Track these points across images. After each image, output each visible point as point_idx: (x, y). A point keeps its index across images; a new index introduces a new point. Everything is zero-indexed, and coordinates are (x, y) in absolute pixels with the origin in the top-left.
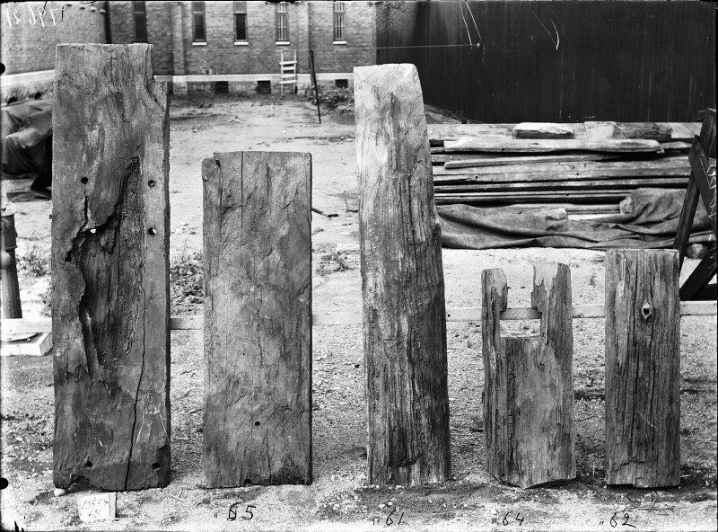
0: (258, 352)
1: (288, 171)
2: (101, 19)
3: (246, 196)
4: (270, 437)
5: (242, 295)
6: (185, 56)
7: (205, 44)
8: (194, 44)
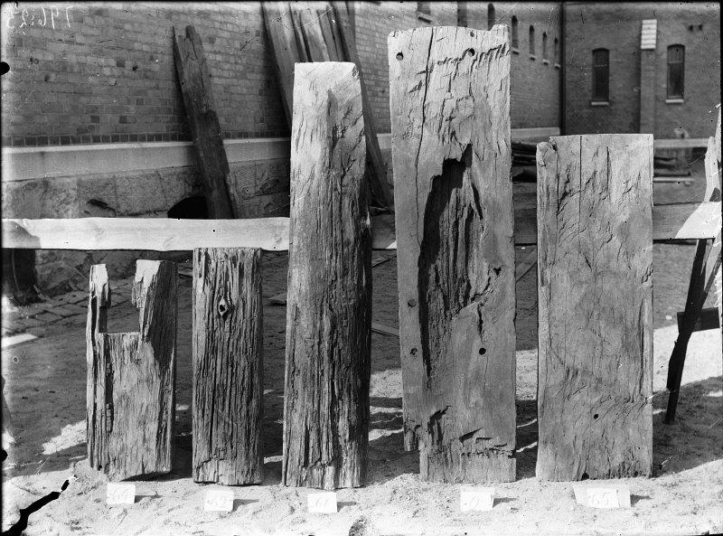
0: (599, 342)
1: (630, 154)
2: (555, 74)
3: (585, 181)
4: (609, 431)
5: (581, 283)
6: (655, 117)
7: (681, 101)
8: (668, 101)
